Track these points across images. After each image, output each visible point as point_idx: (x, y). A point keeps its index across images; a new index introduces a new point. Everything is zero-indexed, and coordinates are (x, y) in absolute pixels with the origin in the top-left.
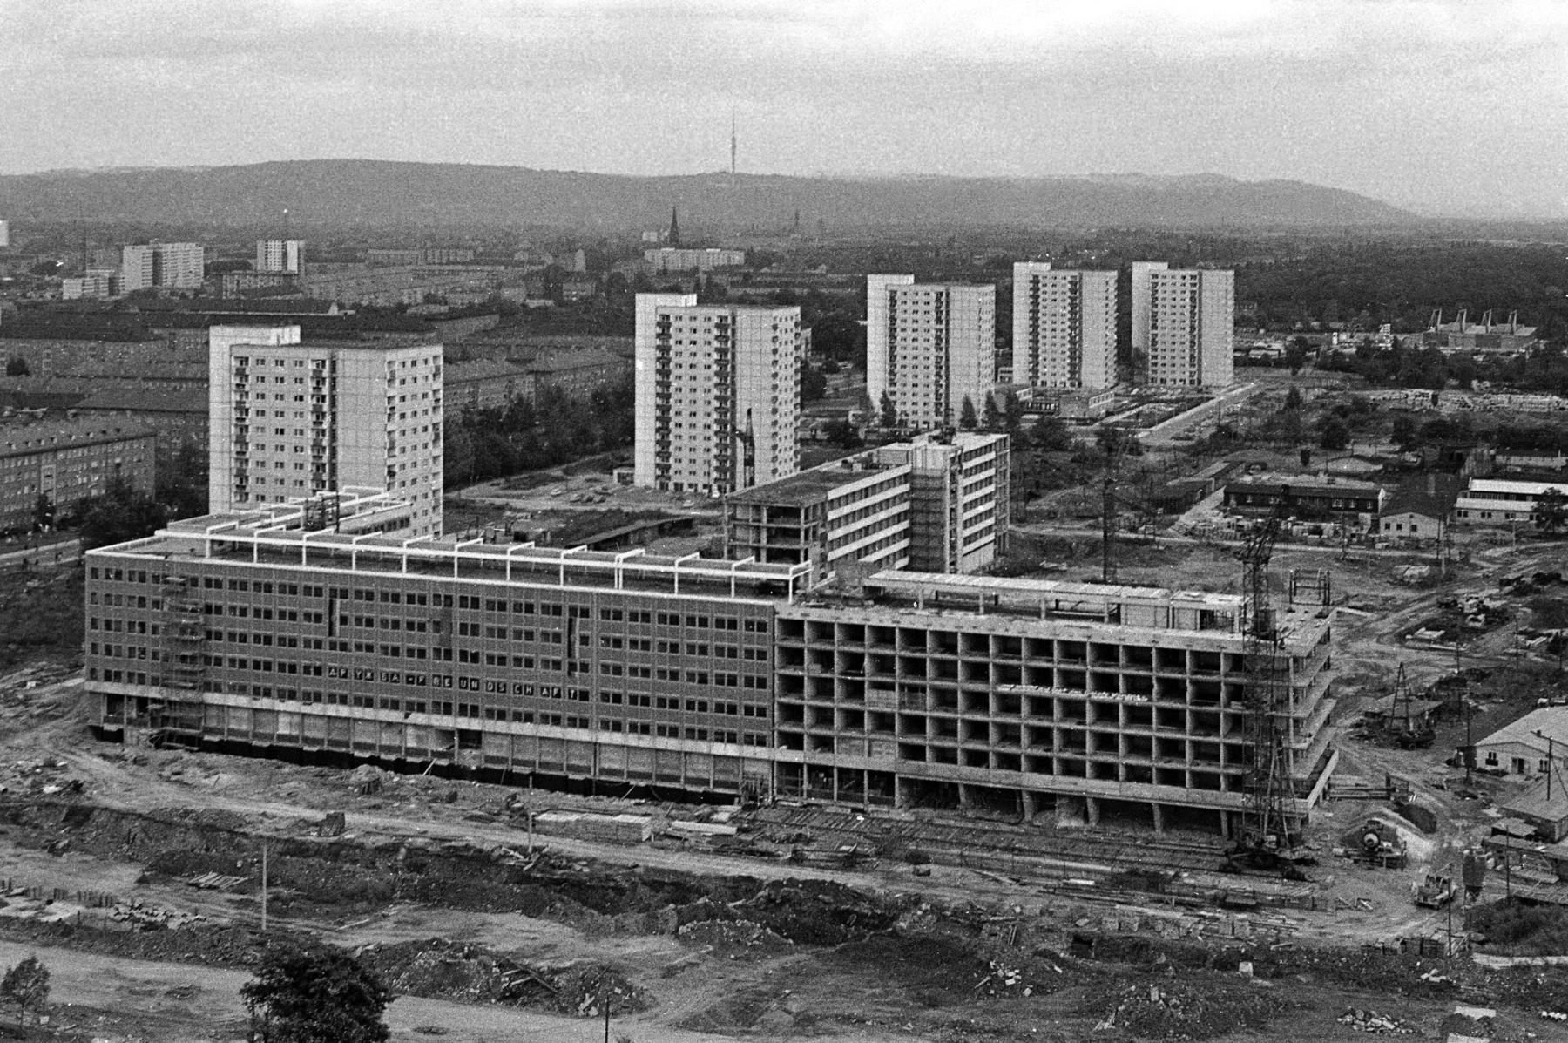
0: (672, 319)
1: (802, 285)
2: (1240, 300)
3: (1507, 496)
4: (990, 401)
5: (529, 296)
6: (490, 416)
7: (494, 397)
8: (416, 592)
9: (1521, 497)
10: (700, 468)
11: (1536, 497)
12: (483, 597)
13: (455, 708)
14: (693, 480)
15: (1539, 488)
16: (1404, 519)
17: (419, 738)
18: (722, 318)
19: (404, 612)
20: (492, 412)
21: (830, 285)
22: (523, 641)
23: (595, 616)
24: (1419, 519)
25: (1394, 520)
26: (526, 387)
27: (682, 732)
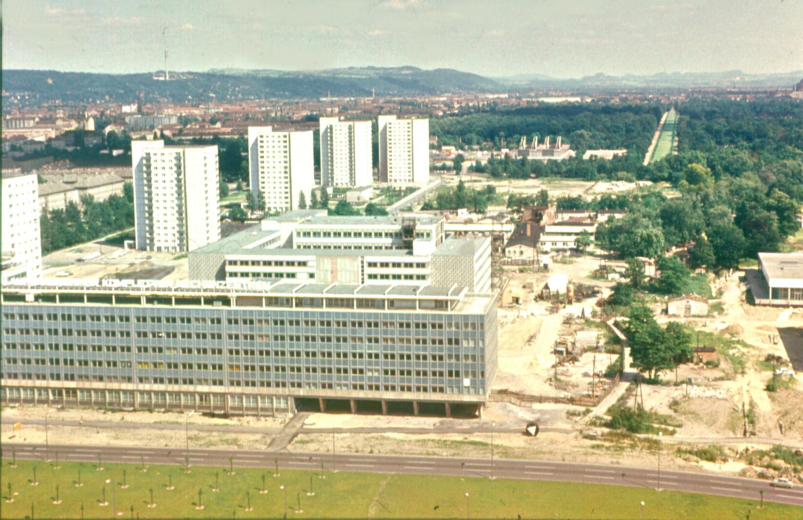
0: (152, 155)
1: (209, 134)
2: (432, 134)
3: (563, 234)
4: (313, 195)
5: (67, 145)
6: (57, 214)
7: (58, 203)
8: (372, 320)
9: (569, 234)
10: (170, 238)
11: (576, 234)
12: (73, 313)
13: (48, 376)
14: (167, 245)
15: (579, 229)
16: (516, 248)
17: (11, 393)
18: (178, 154)
19: (303, 331)
20: (574, 199)
21: (224, 134)
22: (326, 342)
23: (133, 320)
24: (524, 248)
25: (512, 249)
26: (75, 196)
27: (414, 388)
